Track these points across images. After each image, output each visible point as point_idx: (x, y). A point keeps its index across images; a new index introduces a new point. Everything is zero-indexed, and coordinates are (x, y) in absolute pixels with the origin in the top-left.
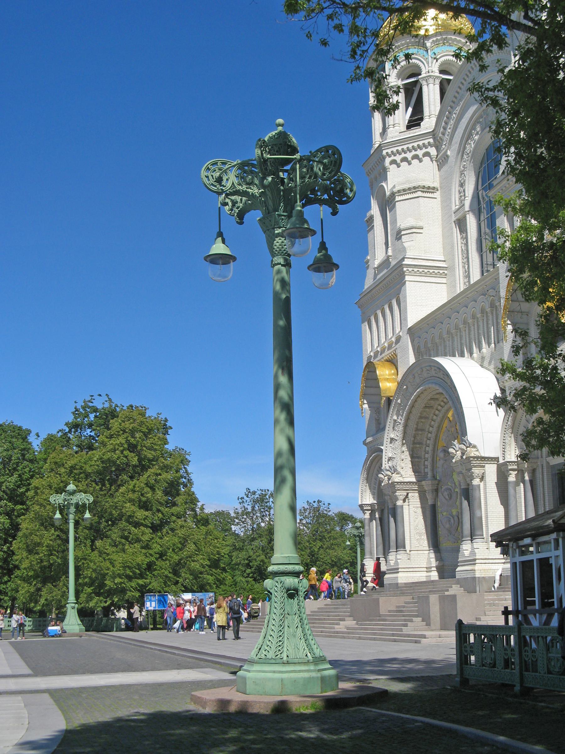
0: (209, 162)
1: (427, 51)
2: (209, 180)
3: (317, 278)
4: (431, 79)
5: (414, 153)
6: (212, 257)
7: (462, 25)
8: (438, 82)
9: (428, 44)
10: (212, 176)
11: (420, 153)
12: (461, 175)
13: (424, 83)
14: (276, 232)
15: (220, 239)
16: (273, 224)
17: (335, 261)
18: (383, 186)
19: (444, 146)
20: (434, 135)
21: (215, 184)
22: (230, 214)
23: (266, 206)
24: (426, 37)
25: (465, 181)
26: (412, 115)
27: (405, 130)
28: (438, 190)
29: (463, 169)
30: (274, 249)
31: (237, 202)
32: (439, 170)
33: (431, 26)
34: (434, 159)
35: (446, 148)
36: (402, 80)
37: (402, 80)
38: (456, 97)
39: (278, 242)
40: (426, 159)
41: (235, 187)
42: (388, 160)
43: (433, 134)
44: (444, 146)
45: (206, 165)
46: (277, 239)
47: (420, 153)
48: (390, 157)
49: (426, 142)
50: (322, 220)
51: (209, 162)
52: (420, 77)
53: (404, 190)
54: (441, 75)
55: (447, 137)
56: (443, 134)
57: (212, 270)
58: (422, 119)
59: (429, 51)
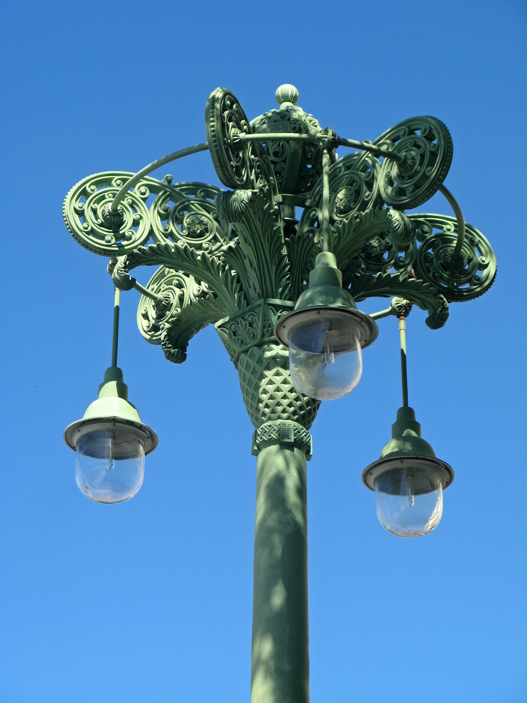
2: (84, 220)
3: (387, 509)
6: (86, 430)
10: (95, 211)
14: (268, 354)
15: (112, 385)
17: (439, 454)
21: (101, 231)
22: (150, 341)
23: (241, 289)
30: (260, 401)
31: (168, 307)
39: (271, 382)
41: (156, 239)
46: (269, 374)
50: (404, 357)
57: (89, 478)
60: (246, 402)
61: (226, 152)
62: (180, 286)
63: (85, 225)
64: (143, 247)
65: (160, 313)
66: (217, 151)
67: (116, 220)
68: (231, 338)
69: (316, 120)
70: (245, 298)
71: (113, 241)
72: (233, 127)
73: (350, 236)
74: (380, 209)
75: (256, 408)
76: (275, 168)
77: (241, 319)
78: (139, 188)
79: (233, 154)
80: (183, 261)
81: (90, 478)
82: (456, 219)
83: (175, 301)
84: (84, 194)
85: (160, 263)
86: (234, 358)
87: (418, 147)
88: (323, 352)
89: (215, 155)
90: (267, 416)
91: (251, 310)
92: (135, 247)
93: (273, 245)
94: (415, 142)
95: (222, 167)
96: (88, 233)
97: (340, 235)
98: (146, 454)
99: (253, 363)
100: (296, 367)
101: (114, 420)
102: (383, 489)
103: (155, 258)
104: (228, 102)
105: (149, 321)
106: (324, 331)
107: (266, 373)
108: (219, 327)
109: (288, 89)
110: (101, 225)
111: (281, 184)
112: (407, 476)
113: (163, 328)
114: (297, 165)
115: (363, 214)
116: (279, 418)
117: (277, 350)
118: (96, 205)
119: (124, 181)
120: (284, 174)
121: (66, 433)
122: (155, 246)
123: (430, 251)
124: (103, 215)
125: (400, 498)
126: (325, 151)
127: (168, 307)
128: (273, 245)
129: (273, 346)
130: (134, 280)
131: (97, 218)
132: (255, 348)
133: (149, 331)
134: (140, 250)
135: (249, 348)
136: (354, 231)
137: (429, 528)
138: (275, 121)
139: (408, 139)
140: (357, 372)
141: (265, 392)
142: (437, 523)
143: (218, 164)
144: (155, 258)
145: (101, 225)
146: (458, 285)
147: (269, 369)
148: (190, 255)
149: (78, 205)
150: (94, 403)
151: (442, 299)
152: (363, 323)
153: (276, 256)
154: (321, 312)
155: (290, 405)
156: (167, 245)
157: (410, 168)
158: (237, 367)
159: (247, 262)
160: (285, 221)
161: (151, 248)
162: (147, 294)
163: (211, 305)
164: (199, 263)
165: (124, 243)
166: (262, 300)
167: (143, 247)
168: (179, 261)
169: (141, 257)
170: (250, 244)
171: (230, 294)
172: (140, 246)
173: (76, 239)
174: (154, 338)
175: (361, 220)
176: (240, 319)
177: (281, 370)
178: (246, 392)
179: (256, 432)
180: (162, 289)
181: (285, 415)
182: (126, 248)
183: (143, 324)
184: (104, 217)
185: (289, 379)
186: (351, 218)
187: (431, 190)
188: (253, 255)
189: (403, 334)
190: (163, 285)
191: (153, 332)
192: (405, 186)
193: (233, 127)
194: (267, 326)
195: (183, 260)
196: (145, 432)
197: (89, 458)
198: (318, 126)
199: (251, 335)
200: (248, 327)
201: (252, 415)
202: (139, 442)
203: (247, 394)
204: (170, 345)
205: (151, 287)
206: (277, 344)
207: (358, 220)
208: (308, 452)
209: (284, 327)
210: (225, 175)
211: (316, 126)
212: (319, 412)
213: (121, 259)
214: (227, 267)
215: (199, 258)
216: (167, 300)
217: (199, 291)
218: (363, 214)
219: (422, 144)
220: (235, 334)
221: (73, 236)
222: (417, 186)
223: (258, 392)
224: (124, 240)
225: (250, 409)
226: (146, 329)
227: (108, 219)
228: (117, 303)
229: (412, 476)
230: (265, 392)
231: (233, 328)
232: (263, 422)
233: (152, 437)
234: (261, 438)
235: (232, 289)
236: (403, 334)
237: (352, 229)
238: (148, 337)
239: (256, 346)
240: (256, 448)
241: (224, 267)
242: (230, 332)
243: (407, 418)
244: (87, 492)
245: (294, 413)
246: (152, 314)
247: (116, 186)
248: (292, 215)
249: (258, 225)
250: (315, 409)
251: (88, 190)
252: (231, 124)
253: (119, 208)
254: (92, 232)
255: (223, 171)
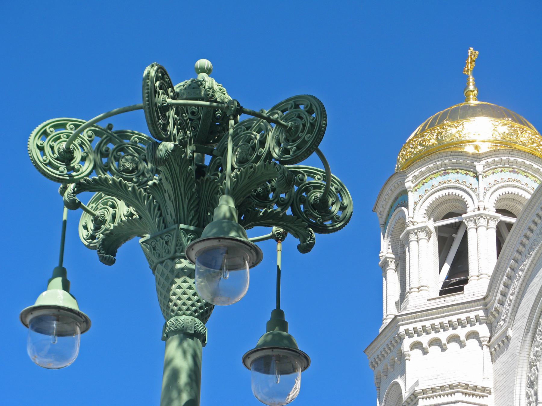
0: (48, 122)
1: (477, 177)
2: (44, 154)
3: (259, 384)
4: (482, 220)
5: (451, 332)
7: (535, 145)
8: (493, 224)
9: (479, 168)
10: (52, 148)
11: (462, 332)
12: (531, 368)
13: (470, 225)
14: (178, 266)
15: (58, 281)
16: (172, 251)
18: (397, 383)
19: (502, 323)
20: (486, 305)
21: (57, 163)
22: (88, 246)
23: (161, 215)
24: (477, 157)
25: (537, 378)
26: (451, 275)
27: (438, 296)
28: (490, 393)
29: (534, 358)
30: (171, 301)
31: (104, 222)
32: (493, 360)
33: (484, 141)
34: (486, 343)
35: (506, 324)
36: (435, 221)
37: (435, 221)
38: (524, 245)
39: (179, 287)
40: (473, 343)
42: (407, 342)
43: (484, 302)
44: (502, 323)
45: (42, 125)
46: (179, 281)
47: (462, 332)
48: (410, 337)
49: (472, 315)
51: (48, 122)
52: (464, 216)
53: (433, 390)
54: (499, 215)
55: (507, 308)
56: (502, 303)
57: (38, 351)
58: (466, 281)
59: (480, 177)
60: (160, 301)
61: (156, 114)
62: (113, 207)
63: (44, 158)
64: (88, 178)
65: (97, 226)
66: (149, 108)
67: (68, 156)
68: (151, 252)
69: (225, 89)
70: (163, 222)
71: (66, 172)
72: (163, 93)
73: (245, 181)
74: (270, 163)
75: (167, 306)
76: (191, 124)
77: (159, 238)
78: (87, 132)
79: (161, 114)
80: (117, 190)
81: (38, 350)
82: (324, 171)
83: (109, 218)
84: (45, 134)
85: (99, 191)
86: (153, 267)
87: (301, 118)
88: (221, 269)
89: (148, 114)
90: (175, 312)
91: (168, 232)
92: (82, 178)
93: (187, 184)
94: (299, 114)
95: (153, 124)
96: (46, 164)
97: (238, 180)
98: (81, 333)
99: (166, 272)
100: (199, 278)
101: (59, 308)
102: (257, 369)
103: (96, 187)
104: (160, 75)
105: (88, 231)
106: (222, 254)
107: (176, 280)
108: (142, 243)
109: (204, 63)
110: (57, 159)
111: (195, 136)
112: (276, 360)
113: (99, 238)
114: (209, 125)
115: (257, 165)
116: (184, 314)
117: (184, 263)
118: (53, 143)
119: (77, 126)
120: (199, 129)
121: (22, 314)
122: (97, 178)
123: (304, 194)
124: (58, 152)
125: (270, 376)
126: (232, 117)
127: (104, 222)
128: (187, 184)
129: (183, 260)
130: (80, 203)
131: (53, 153)
132: (169, 261)
133: (88, 239)
134: (85, 180)
135: (164, 261)
136: (249, 177)
137: (289, 400)
138: (194, 88)
139: (295, 111)
140: (245, 286)
141: (174, 294)
142: (295, 396)
143: (150, 122)
144: (96, 187)
145: (57, 159)
146: (323, 222)
147: (178, 277)
148: (123, 186)
149: (39, 142)
150: (44, 293)
151: (310, 231)
152: (252, 250)
153: (189, 192)
154: (221, 240)
155: (193, 305)
156: (106, 178)
157: (294, 134)
158: (154, 273)
159: (166, 195)
160: (196, 165)
161: (94, 179)
162: (88, 211)
163: (137, 224)
164: (130, 193)
165: (74, 174)
166: (177, 225)
167: (88, 178)
168: (115, 191)
169: (87, 186)
170: (170, 182)
171: (151, 215)
172: (85, 178)
173: (37, 168)
174: (91, 245)
175: (255, 170)
176: (158, 238)
177: (188, 279)
178: (160, 293)
179: (166, 324)
180: (100, 208)
181: (189, 312)
182: (75, 177)
183: (83, 234)
184: (59, 154)
185: (194, 286)
186: (247, 169)
187: (308, 152)
188: (171, 188)
189: (279, 254)
190: (100, 205)
191: (91, 240)
192: (289, 147)
193: (163, 93)
194: (179, 245)
195: (117, 190)
196: (81, 317)
197: (38, 334)
198: (226, 94)
199: (167, 251)
200: (165, 245)
201: (164, 311)
202: (76, 324)
203: (161, 294)
204: (103, 252)
205: (91, 205)
206: (185, 259)
207: (252, 169)
208: (203, 341)
209: (193, 249)
210: (154, 130)
211: (224, 94)
212: (213, 311)
213: (71, 186)
214: (151, 197)
215: (130, 189)
216: (103, 217)
217: (128, 212)
218: (257, 165)
219: (304, 117)
220: (154, 248)
221: (35, 166)
222: (298, 148)
223: (169, 294)
224: (74, 171)
225: (162, 306)
226: (85, 237)
227: (62, 155)
228: (65, 217)
229: (279, 361)
230: (174, 294)
231: (153, 244)
232: (171, 317)
233: (87, 321)
234: (170, 329)
235: (154, 214)
236: (279, 254)
237: (247, 177)
238: (87, 243)
239: (169, 259)
240: (165, 335)
241: (149, 197)
242: (150, 247)
243: (278, 319)
244: (35, 360)
245: (196, 311)
246: (91, 226)
247: (70, 128)
248: (202, 160)
249: (177, 168)
250: (211, 309)
251: (48, 131)
252: (161, 91)
253: (71, 147)
254: (50, 164)
255: (153, 127)
